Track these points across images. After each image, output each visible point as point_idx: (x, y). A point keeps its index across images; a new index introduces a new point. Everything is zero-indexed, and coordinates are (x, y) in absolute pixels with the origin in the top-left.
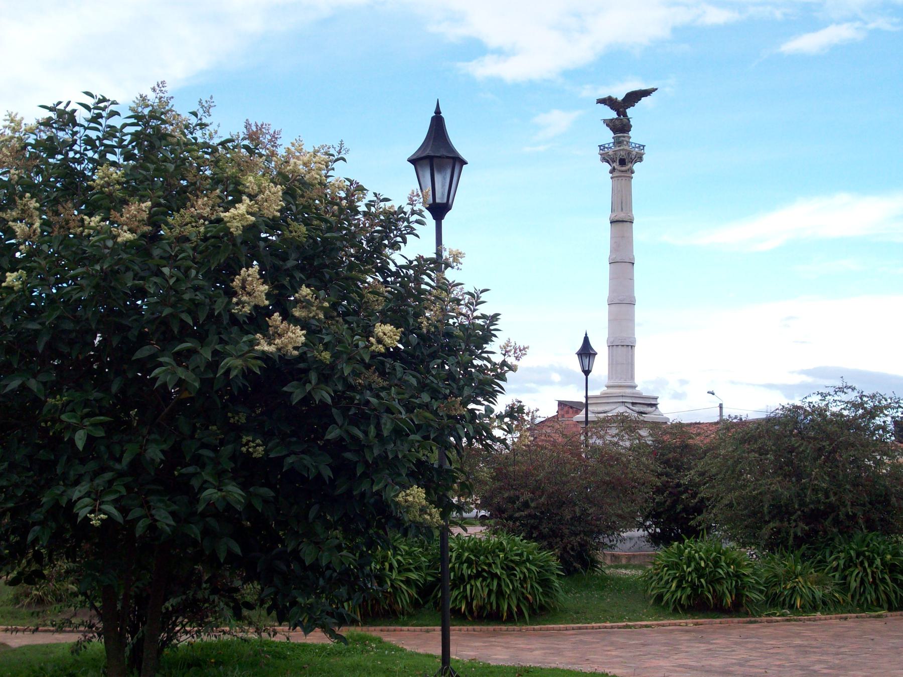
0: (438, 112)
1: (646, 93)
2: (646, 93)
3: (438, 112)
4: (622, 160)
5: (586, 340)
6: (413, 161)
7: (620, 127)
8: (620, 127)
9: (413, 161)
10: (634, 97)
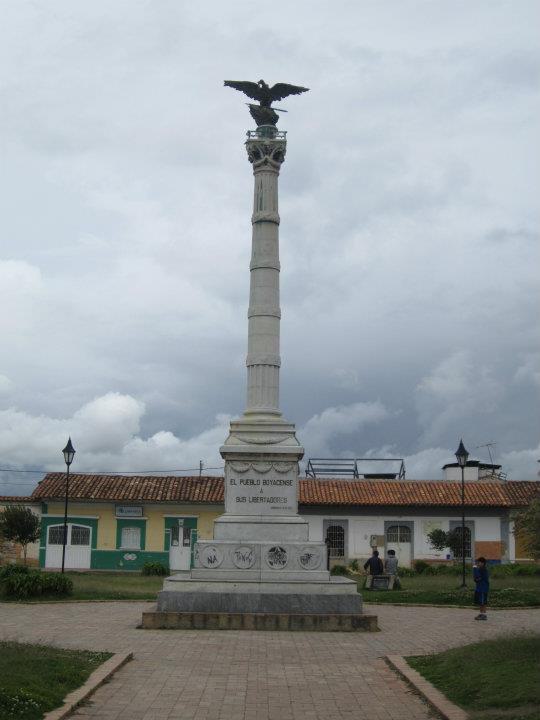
1: (296, 90)
2: (296, 90)
4: (267, 153)
5: (461, 445)
6: (64, 451)
7: (265, 117)
8: (265, 117)
9: (64, 451)
10: (283, 90)
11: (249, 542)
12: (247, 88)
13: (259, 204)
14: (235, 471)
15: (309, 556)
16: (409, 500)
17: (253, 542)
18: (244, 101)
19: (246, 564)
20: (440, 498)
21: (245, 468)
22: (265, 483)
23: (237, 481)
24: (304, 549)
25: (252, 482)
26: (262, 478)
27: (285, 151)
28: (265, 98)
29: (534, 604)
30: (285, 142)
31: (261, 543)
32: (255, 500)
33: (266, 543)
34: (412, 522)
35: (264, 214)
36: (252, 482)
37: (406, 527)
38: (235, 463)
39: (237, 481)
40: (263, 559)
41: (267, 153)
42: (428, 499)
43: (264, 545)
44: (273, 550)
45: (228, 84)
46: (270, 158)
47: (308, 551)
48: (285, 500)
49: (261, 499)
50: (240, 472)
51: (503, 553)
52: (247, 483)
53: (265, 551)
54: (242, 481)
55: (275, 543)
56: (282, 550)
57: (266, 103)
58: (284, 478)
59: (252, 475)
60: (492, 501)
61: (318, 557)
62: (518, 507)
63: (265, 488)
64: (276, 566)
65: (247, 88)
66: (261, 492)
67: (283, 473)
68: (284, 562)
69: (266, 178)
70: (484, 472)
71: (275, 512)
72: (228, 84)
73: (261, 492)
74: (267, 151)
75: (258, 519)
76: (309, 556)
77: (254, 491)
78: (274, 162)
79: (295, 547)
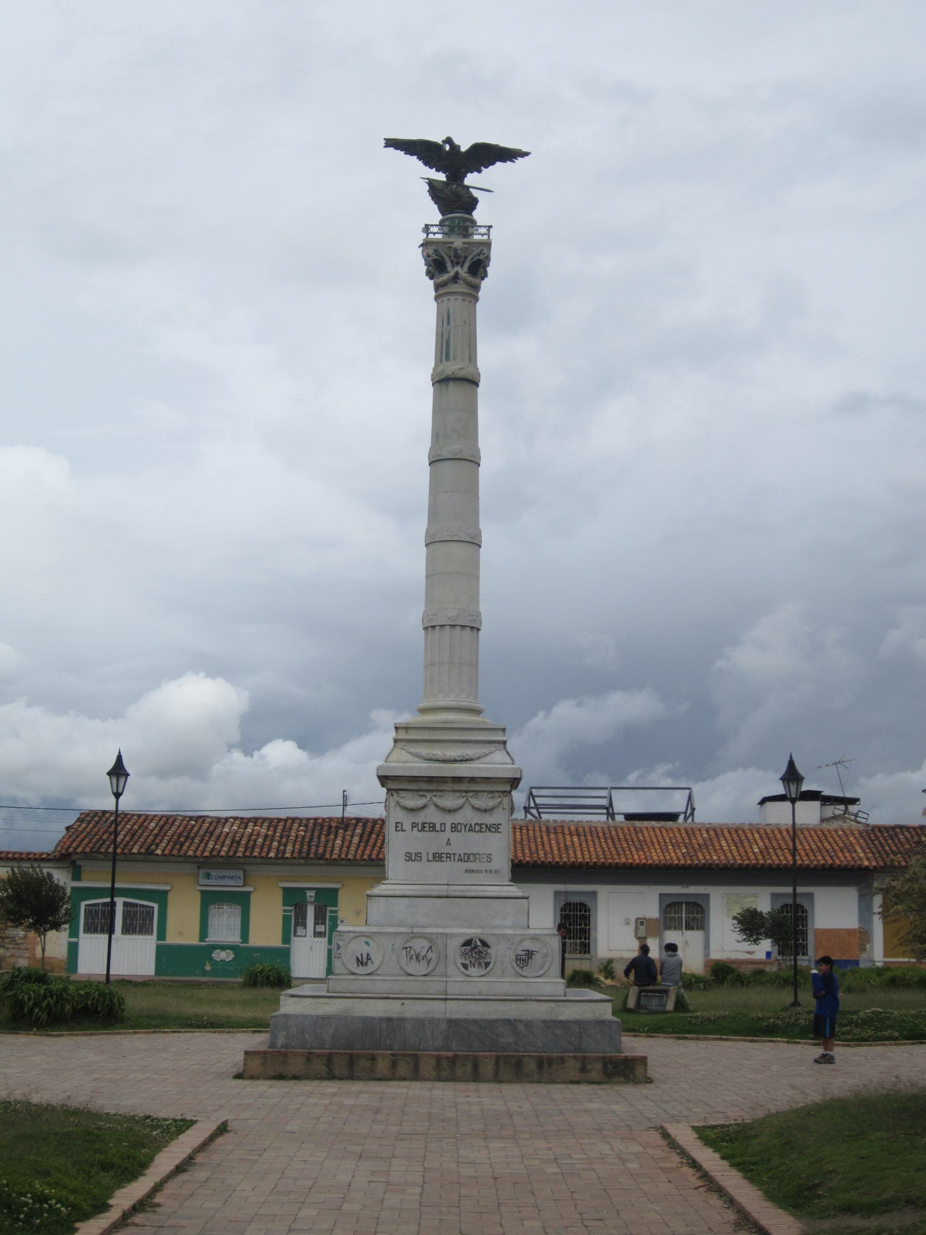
0: (791, 757)
3: (791, 757)
4: (458, 263)
7: (454, 201)
8: (454, 201)
10: (487, 155)
12: (425, 151)
13: (444, 349)
14: (404, 808)
16: (702, 858)
17: (434, 930)
18: (418, 174)
19: (421, 968)
20: (755, 854)
21: (420, 802)
22: (455, 828)
23: (407, 826)
24: (521, 941)
25: (433, 827)
26: (449, 820)
27: (488, 258)
28: (454, 168)
30: (488, 244)
31: (448, 931)
32: (437, 857)
33: (455, 931)
34: (707, 896)
35: (452, 368)
36: (433, 827)
37: (699, 905)
38: (403, 794)
39: (407, 826)
40: (451, 958)
41: (458, 263)
43: (452, 936)
44: (468, 943)
45: (392, 143)
46: (463, 271)
47: (527, 945)
49: (449, 856)
51: (863, 949)
53: (454, 946)
54: (414, 825)
55: (472, 932)
56: (485, 944)
57: (456, 176)
58: (488, 819)
59: (431, 815)
60: (843, 859)
61: (546, 955)
62: (888, 869)
63: (454, 836)
64: (473, 971)
65: (425, 151)
66: (448, 843)
68: (487, 964)
69: (456, 304)
70: (830, 810)
72: (392, 143)
73: (448, 843)
74: (458, 260)
75: (443, 890)
76: (530, 954)
78: (470, 278)
79: (506, 938)
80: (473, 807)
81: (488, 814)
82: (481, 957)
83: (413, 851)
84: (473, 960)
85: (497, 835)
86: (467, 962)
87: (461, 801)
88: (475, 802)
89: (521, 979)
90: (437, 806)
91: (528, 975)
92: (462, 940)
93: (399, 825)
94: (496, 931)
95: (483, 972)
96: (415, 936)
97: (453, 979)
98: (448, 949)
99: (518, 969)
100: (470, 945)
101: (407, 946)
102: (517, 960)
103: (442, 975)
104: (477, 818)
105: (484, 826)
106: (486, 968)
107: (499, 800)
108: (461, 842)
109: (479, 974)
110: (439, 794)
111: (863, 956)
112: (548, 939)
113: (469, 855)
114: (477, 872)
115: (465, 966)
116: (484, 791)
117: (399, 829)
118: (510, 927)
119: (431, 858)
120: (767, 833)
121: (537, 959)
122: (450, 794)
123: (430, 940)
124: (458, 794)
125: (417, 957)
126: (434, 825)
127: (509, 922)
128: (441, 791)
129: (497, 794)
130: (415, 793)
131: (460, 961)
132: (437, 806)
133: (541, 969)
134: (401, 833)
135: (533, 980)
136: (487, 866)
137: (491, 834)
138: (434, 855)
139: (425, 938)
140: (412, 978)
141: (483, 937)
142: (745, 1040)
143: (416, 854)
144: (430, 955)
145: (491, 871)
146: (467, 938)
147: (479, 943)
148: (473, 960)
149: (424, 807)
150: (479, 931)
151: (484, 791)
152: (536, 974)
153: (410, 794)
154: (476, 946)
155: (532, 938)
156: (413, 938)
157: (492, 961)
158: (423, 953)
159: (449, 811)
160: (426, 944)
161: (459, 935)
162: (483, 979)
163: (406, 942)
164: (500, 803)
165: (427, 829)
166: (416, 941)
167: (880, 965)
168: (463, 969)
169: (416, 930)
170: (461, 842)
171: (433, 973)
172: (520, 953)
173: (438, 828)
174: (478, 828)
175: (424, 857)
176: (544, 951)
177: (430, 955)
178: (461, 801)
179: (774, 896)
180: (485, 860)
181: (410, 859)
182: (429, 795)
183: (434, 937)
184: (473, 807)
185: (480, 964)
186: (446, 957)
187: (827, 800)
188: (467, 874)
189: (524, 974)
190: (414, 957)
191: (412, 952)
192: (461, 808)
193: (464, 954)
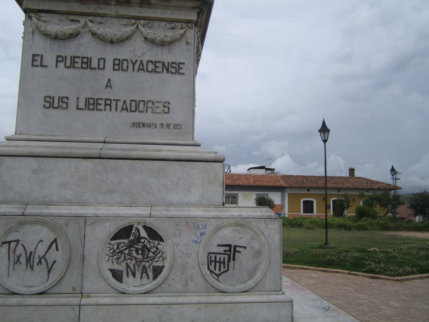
0: (324, 120)
3: (324, 120)
11: (45, 211)
14: (46, 35)
15: (232, 251)
16: (236, 183)
17: (64, 210)
19: (37, 280)
20: (251, 182)
21: (68, 28)
22: (119, 65)
23: (50, 59)
24: (218, 229)
25: (87, 63)
26: (111, 54)
29: (2, 153)
31: (89, 211)
32: (92, 104)
34: (238, 194)
36: (87, 63)
37: (235, 197)
38: (45, 17)
39: (50, 59)
40: (91, 259)
42: (246, 183)
43: (97, 219)
44: (124, 232)
47: (228, 236)
48: (167, 105)
49: (108, 103)
50: (56, 38)
51: (282, 210)
52: (72, 65)
53: (99, 238)
54: (60, 59)
56: (153, 234)
58: (165, 56)
59: (86, 47)
60: (277, 184)
61: (259, 253)
62: (291, 187)
63: (118, 77)
64: (131, 283)
66: (109, 85)
67: (163, 44)
68: (157, 271)
70: (269, 172)
71: (144, 135)
73: (109, 85)
75: (95, 149)
76: (232, 251)
77: (90, 84)
79: (192, 223)
80: (146, 38)
81: (165, 49)
82: (145, 257)
83: (56, 94)
84: (132, 264)
85: (178, 77)
86: (122, 267)
87: (129, 29)
88: (146, 31)
89: (216, 298)
90: (94, 34)
91: (229, 288)
92: (112, 228)
93: (39, 59)
94: (173, 212)
95: (150, 285)
96: (25, 220)
97: (92, 300)
98: (88, 245)
99: (212, 279)
100: (127, 237)
101: (9, 239)
102: (210, 262)
103: (74, 292)
104: (150, 54)
105: (160, 65)
106: (155, 278)
107: (182, 31)
108: (125, 86)
109: (142, 289)
110: (99, 19)
111: (282, 212)
112: (262, 225)
113: (138, 103)
114: (149, 126)
115: (117, 275)
116: (161, 20)
117: (38, 63)
118: (197, 205)
119: (82, 105)
120: (255, 177)
121: (244, 258)
122: (115, 20)
123: (54, 228)
124: (125, 21)
125: (28, 260)
126: (89, 60)
127: (194, 196)
128: (103, 16)
129: (179, 25)
130: (63, 17)
131: (107, 266)
132: (94, 34)
133: (251, 277)
134: (40, 70)
135: (238, 298)
136: (165, 119)
137: (169, 75)
138: (87, 100)
139: (44, 224)
140: (14, 300)
141: (150, 223)
142: (318, 270)
143: (61, 99)
144: (53, 255)
145: (168, 126)
146: (125, 223)
147: (143, 233)
148: (132, 264)
149: (73, 36)
150: (144, 211)
151: (161, 20)
152: (242, 287)
153: (56, 17)
154: (140, 238)
155: (236, 225)
156: (22, 224)
157: (167, 264)
158: (41, 251)
159: (112, 42)
160: (46, 235)
161: (108, 218)
162: (151, 299)
163: (9, 231)
164: (182, 35)
165: (79, 65)
166: (29, 228)
167: (287, 216)
168: (113, 281)
169: (30, 210)
170: (125, 86)
171: (55, 290)
172: (216, 249)
173: (94, 64)
174: (151, 67)
175: (72, 103)
176: (256, 245)
177: (53, 255)
178: (129, 29)
179: (257, 194)
180: (160, 110)
181: (52, 106)
182: (83, 20)
183: (62, 222)
184: (146, 38)
185: (144, 270)
186: (83, 258)
187: (267, 169)
188: (134, 129)
189: (222, 286)
190: (23, 260)
191: (20, 250)
192: (128, 38)
193: (116, 253)
